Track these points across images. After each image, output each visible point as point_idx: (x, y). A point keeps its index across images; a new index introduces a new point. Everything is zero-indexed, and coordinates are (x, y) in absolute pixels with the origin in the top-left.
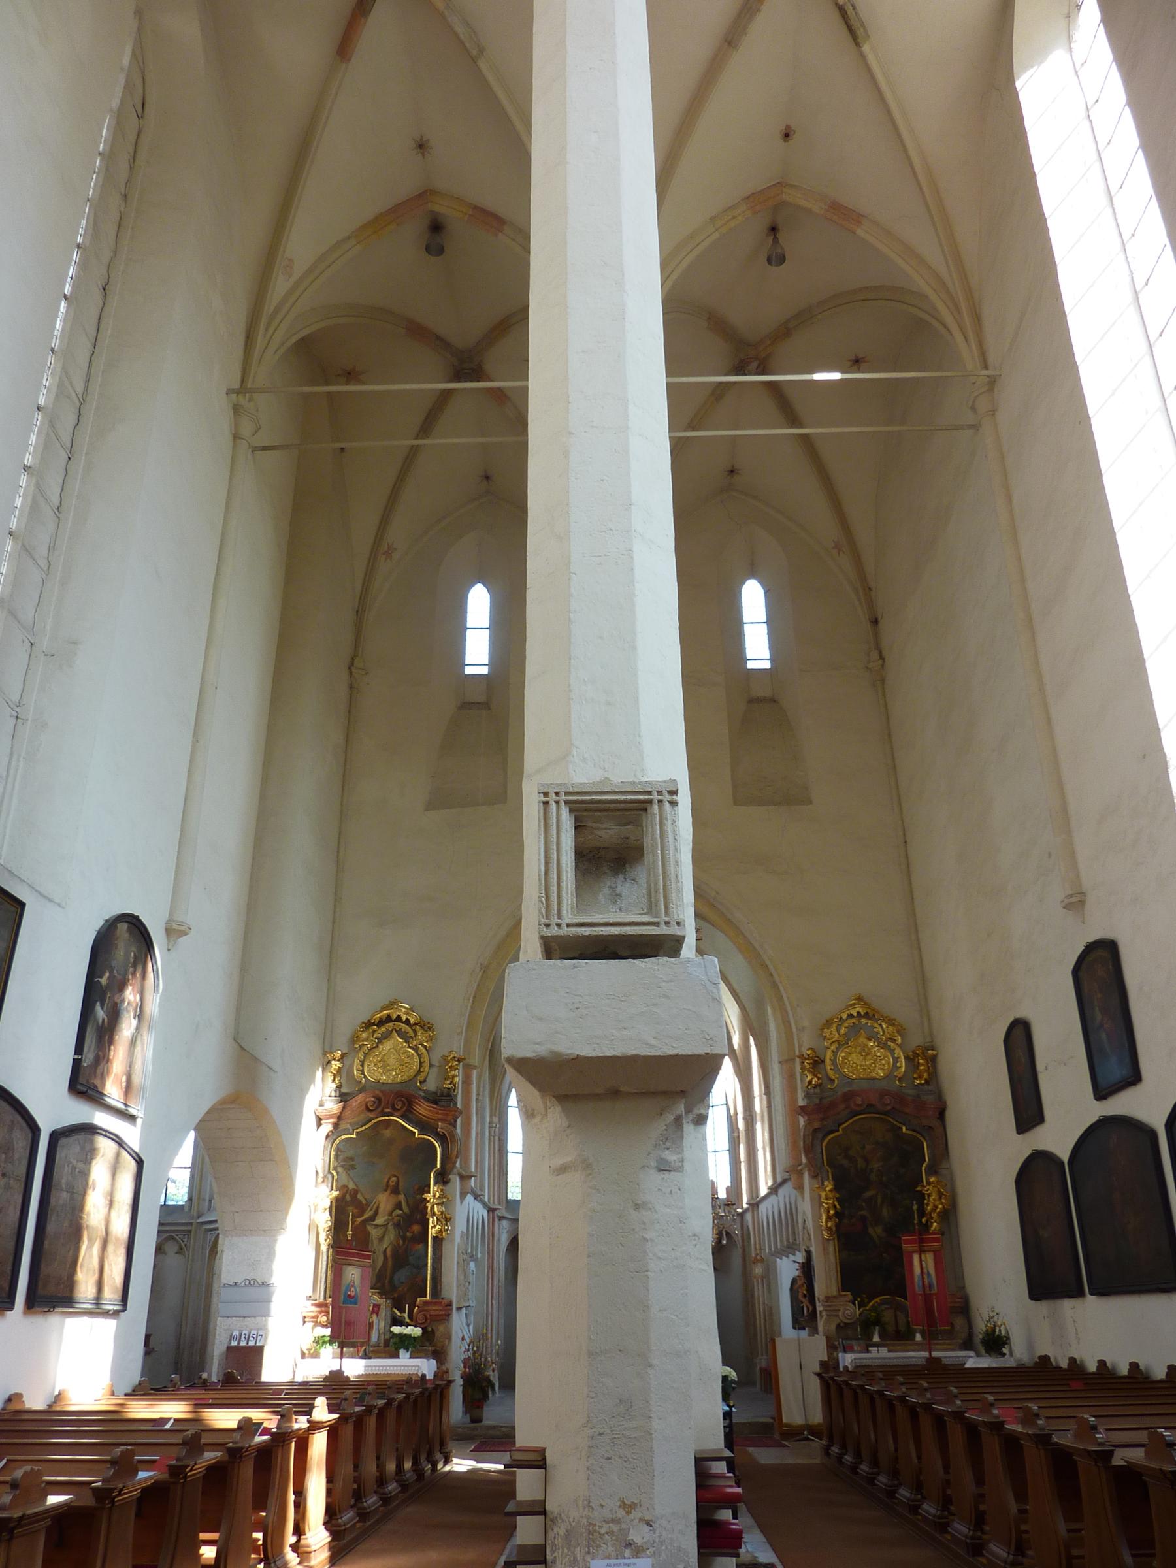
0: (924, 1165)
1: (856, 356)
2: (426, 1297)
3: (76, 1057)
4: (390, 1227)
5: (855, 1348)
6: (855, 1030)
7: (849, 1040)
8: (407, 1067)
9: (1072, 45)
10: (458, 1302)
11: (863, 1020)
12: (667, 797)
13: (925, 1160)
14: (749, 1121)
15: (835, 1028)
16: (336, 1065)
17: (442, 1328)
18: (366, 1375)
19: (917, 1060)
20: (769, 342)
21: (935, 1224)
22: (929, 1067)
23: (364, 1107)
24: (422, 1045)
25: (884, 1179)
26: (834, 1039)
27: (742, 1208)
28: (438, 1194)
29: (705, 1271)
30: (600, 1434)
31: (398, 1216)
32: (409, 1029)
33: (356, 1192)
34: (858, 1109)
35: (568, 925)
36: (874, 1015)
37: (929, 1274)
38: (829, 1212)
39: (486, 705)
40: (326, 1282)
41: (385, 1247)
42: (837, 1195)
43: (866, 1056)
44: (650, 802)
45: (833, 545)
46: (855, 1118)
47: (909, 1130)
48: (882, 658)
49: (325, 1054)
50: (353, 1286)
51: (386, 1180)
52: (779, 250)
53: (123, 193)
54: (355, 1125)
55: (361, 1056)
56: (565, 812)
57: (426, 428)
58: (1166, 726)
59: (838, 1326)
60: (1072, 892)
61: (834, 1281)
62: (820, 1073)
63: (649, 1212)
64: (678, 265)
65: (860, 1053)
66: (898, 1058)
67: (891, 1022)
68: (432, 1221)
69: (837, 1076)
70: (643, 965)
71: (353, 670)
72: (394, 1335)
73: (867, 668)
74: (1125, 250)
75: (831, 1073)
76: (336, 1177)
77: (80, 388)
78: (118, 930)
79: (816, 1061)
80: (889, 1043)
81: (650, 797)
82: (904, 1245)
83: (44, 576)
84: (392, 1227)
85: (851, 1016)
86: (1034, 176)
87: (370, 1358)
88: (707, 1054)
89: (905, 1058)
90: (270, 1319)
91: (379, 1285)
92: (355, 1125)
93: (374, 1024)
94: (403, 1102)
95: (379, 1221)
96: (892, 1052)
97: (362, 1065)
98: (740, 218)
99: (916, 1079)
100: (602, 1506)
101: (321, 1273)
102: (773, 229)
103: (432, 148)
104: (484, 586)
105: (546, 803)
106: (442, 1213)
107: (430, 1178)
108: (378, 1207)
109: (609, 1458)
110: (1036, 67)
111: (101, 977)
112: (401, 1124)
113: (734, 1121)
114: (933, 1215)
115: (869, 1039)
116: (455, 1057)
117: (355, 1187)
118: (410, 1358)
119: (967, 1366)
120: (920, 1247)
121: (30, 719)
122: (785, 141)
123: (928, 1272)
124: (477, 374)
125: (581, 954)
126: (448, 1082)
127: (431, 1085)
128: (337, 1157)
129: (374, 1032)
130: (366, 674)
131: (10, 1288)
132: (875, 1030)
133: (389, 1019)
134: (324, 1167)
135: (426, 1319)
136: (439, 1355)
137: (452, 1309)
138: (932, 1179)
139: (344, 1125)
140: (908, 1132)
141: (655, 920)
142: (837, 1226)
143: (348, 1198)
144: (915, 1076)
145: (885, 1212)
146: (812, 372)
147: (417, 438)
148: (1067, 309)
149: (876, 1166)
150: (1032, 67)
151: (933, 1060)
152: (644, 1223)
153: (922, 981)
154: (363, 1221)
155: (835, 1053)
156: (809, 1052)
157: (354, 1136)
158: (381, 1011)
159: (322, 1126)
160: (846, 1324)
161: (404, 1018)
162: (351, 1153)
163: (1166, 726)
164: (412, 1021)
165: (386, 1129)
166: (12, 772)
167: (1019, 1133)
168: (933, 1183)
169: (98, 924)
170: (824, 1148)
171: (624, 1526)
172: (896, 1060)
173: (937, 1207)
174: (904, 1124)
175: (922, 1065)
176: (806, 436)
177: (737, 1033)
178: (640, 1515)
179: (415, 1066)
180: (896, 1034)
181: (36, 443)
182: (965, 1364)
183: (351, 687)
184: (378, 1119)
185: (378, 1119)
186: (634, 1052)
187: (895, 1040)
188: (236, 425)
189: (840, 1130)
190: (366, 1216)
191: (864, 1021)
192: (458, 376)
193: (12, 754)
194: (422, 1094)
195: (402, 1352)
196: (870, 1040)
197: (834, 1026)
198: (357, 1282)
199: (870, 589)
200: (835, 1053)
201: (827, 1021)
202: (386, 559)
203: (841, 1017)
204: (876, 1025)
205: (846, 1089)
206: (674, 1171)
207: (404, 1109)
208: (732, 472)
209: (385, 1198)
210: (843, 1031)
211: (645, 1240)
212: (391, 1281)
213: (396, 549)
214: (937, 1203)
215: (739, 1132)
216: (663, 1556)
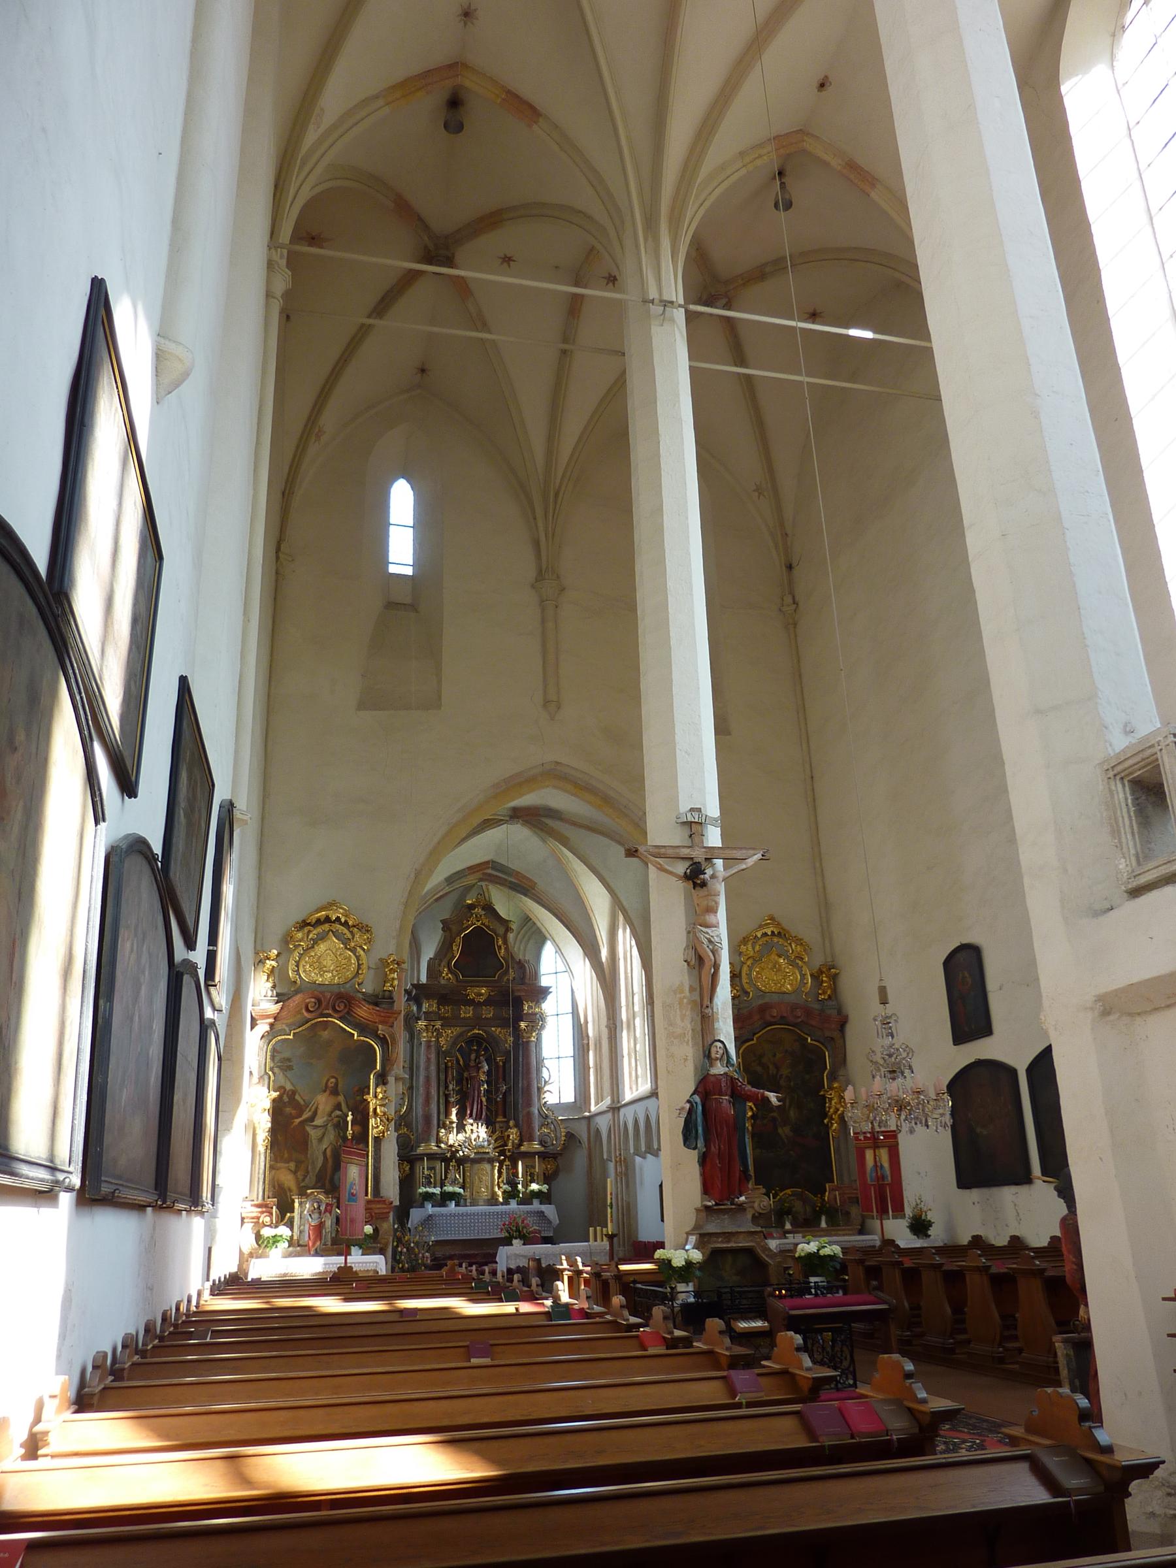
3: (211, 948)
4: (330, 1127)
5: (775, 1235)
6: (768, 948)
8: (344, 968)
9: (1115, 64)
13: (826, 1068)
14: (613, 1029)
16: (270, 964)
18: (323, 1272)
24: (361, 947)
25: (792, 1084)
27: (590, 1112)
28: (380, 1096)
31: (337, 1116)
32: (346, 931)
33: (294, 1093)
34: (772, 1020)
36: (785, 935)
37: (882, 1166)
39: (413, 607)
40: (264, 1182)
41: (324, 1147)
45: (755, 488)
47: (814, 1040)
49: (257, 953)
52: (787, 197)
57: (382, 307)
64: (710, 194)
65: (772, 969)
67: (799, 941)
68: (372, 1122)
71: (280, 555)
73: (780, 610)
74: (1164, 269)
75: (746, 986)
80: (797, 961)
84: (332, 1128)
85: (765, 934)
86: (1079, 181)
89: (811, 975)
90: (217, 1219)
93: (309, 924)
94: (345, 1003)
95: (318, 1121)
97: (297, 966)
98: (765, 158)
99: (821, 994)
101: (259, 1173)
103: (477, 19)
104: (408, 481)
106: (385, 1114)
107: (370, 1079)
108: (317, 1108)
110: (1080, 76)
112: (340, 1026)
113: (584, 1029)
114: (834, 1116)
115: (780, 956)
116: (394, 960)
117: (292, 1088)
118: (362, 1255)
123: (881, 1164)
124: (449, 262)
126: (389, 984)
127: (367, 988)
128: (273, 1058)
129: (309, 932)
130: (293, 560)
132: (785, 948)
133: (328, 920)
134: (260, 1067)
143: (286, 1098)
144: (820, 992)
146: (848, 327)
147: (369, 316)
148: (1110, 313)
150: (1077, 75)
151: (834, 978)
153: (825, 906)
154: (300, 1122)
155: (750, 968)
157: (291, 1037)
159: (256, 1028)
160: (760, 1214)
162: (287, 1055)
164: (350, 923)
165: (325, 1029)
167: (955, 1044)
172: (803, 976)
173: (838, 1110)
174: (809, 1035)
175: (826, 982)
176: (748, 377)
177: (606, 946)
179: (353, 967)
184: (316, 1020)
185: (316, 1020)
187: (803, 959)
190: (305, 1116)
191: (775, 939)
192: (429, 259)
196: (781, 957)
199: (786, 534)
203: (756, 936)
204: (786, 944)
205: (761, 1002)
209: (324, 1099)
210: (757, 948)
213: (325, 432)
214: (838, 1106)
215: (588, 1040)
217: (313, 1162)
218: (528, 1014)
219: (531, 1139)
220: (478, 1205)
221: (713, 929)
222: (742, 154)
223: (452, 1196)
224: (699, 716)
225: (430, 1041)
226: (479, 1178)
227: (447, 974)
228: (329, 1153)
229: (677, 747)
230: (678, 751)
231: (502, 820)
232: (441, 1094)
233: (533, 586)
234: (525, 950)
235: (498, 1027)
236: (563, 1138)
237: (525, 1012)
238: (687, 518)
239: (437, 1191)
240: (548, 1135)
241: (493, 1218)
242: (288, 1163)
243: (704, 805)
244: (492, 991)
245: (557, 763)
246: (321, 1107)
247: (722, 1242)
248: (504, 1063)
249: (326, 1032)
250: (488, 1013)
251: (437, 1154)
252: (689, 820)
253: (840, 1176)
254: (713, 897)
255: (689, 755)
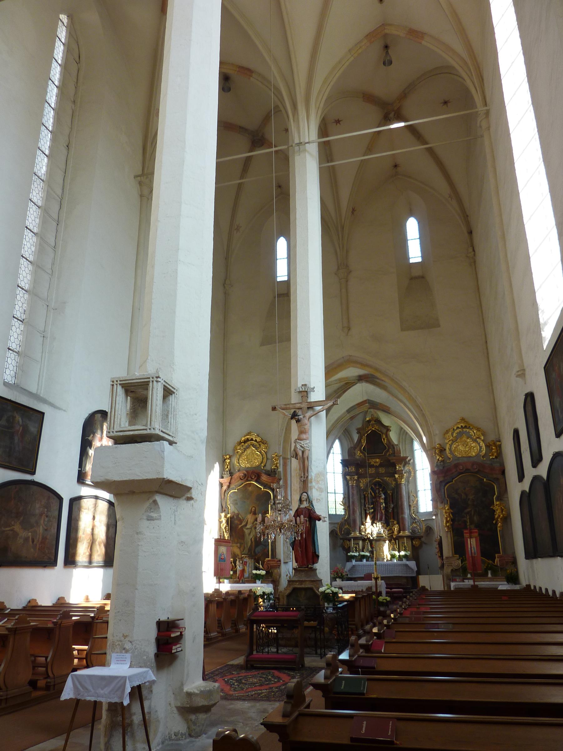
0: (495, 496)
1: (444, 100)
2: (269, 558)
3: (79, 469)
5: (457, 580)
6: (460, 435)
7: (457, 439)
10: (284, 559)
11: (464, 429)
12: (155, 379)
13: (495, 494)
15: (451, 434)
17: (276, 571)
19: (491, 447)
20: (398, 101)
21: (500, 524)
22: (497, 450)
23: (239, 479)
26: (450, 439)
29: (187, 555)
30: (118, 612)
35: (116, 432)
36: (470, 427)
37: (474, 548)
38: (447, 519)
42: (452, 511)
43: (466, 446)
44: (149, 382)
46: (460, 476)
48: (474, 251)
50: (223, 554)
51: (250, 509)
53: (73, 100)
54: (236, 486)
55: (238, 456)
56: (119, 388)
58: (538, 289)
59: (452, 570)
60: (519, 370)
61: (450, 550)
62: (443, 455)
63: (142, 535)
66: (482, 446)
67: (478, 429)
69: (452, 456)
70: (139, 446)
71: (225, 286)
72: (253, 574)
75: (449, 455)
76: (230, 508)
77: (59, 192)
78: (96, 417)
79: (441, 450)
80: (478, 440)
81: (149, 380)
82: (465, 535)
83: (50, 277)
87: (245, 583)
88: (157, 478)
91: (249, 553)
92: (236, 486)
93: (242, 442)
95: (248, 526)
96: (479, 444)
99: (490, 456)
100: (117, 636)
102: (386, 47)
105: (113, 385)
108: (248, 520)
109: (120, 620)
111: (89, 437)
112: (256, 485)
119: (499, 589)
120: (470, 535)
121: (49, 337)
122: (381, 3)
125: (124, 442)
127: (268, 468)
129: (242, 446)
131: (55, 558)
132: (470, 434)
133: (248, 440)
135: (268, 568)
136: (275, 583)
137: (281, 563)
138: (498, 503)
139: (232, 486)
140: (487, 481)
141: (146, 428)
142: (451, 525)
144: (490, 454)
145: (475, 518)
149: (471, 497)
151: (500, 446)
152: (139, 539)
155: (451, 446)
156: (438, 446)
157: (236, 491)
158: (245, 436)
160: (456, 569)
161: (254, 439)
163: (538, 289)
164: (258, 441)
165: (250, 487)
166: (43, 359)
168: (498, 504)
169: (86, 415)
170: (445, 490)
171: (123, 643)
173: (500, 516)
174: (485, 477)
175: (494, 449)
178: (128, 639)
180: (481, 435)
181: (39, 223)
182: (498, 588)
183: (225, 293)
184: (246, 483)
186: (133, 478)
188: (141, 191)
189: (454, 481)
191: (465, 430)
193: (42, 352)
194: (264, 471)
195: (257, 581)
197: (450, 433)
198: (225, 552)
200: (451, 446)
201: (447, 431)
202: (237, 232)
206: (156, 520)
207: (256, 478)
208: (396, 166)
209: (250, 517)
210: (455, 435)
211: (138, 545)
212: (254, 551)
213: (241, 227)
214: (500, 514)
216: (136, 653)
217: (247, 543)
218: (399, 470)
219: (404, 530)
220: (379, 561)
221: (304, 441)
222: (350, 51)
223: (364, 557)
224: (309, 340)
225: (353, 485)
226: (379, 548)
227: (360, 454)
228: (253, 540)
229: (298, 356)
230: (298, 358)
231: (354, 382)
232: (362, 509)
233: (336, 274)
234: (405, 438)
235: (387, 477)
236: (424, 529)
237: (397, 469)
238: (308, 246)
239: (357, 554)
240: (416, 527)
241: (398, 567)
242: (237, 544)
243: (310, 382)
244: (382, 460)
245: (350, 356)
246: (249, 520)
247: (298, 585)
248: (392, 494)
249: (250, 488)
250: (382, 470)
251: (358, 537)
252: (300, 390)
253: (504, 551)
254: (303, 426)
255: (304, 359)
